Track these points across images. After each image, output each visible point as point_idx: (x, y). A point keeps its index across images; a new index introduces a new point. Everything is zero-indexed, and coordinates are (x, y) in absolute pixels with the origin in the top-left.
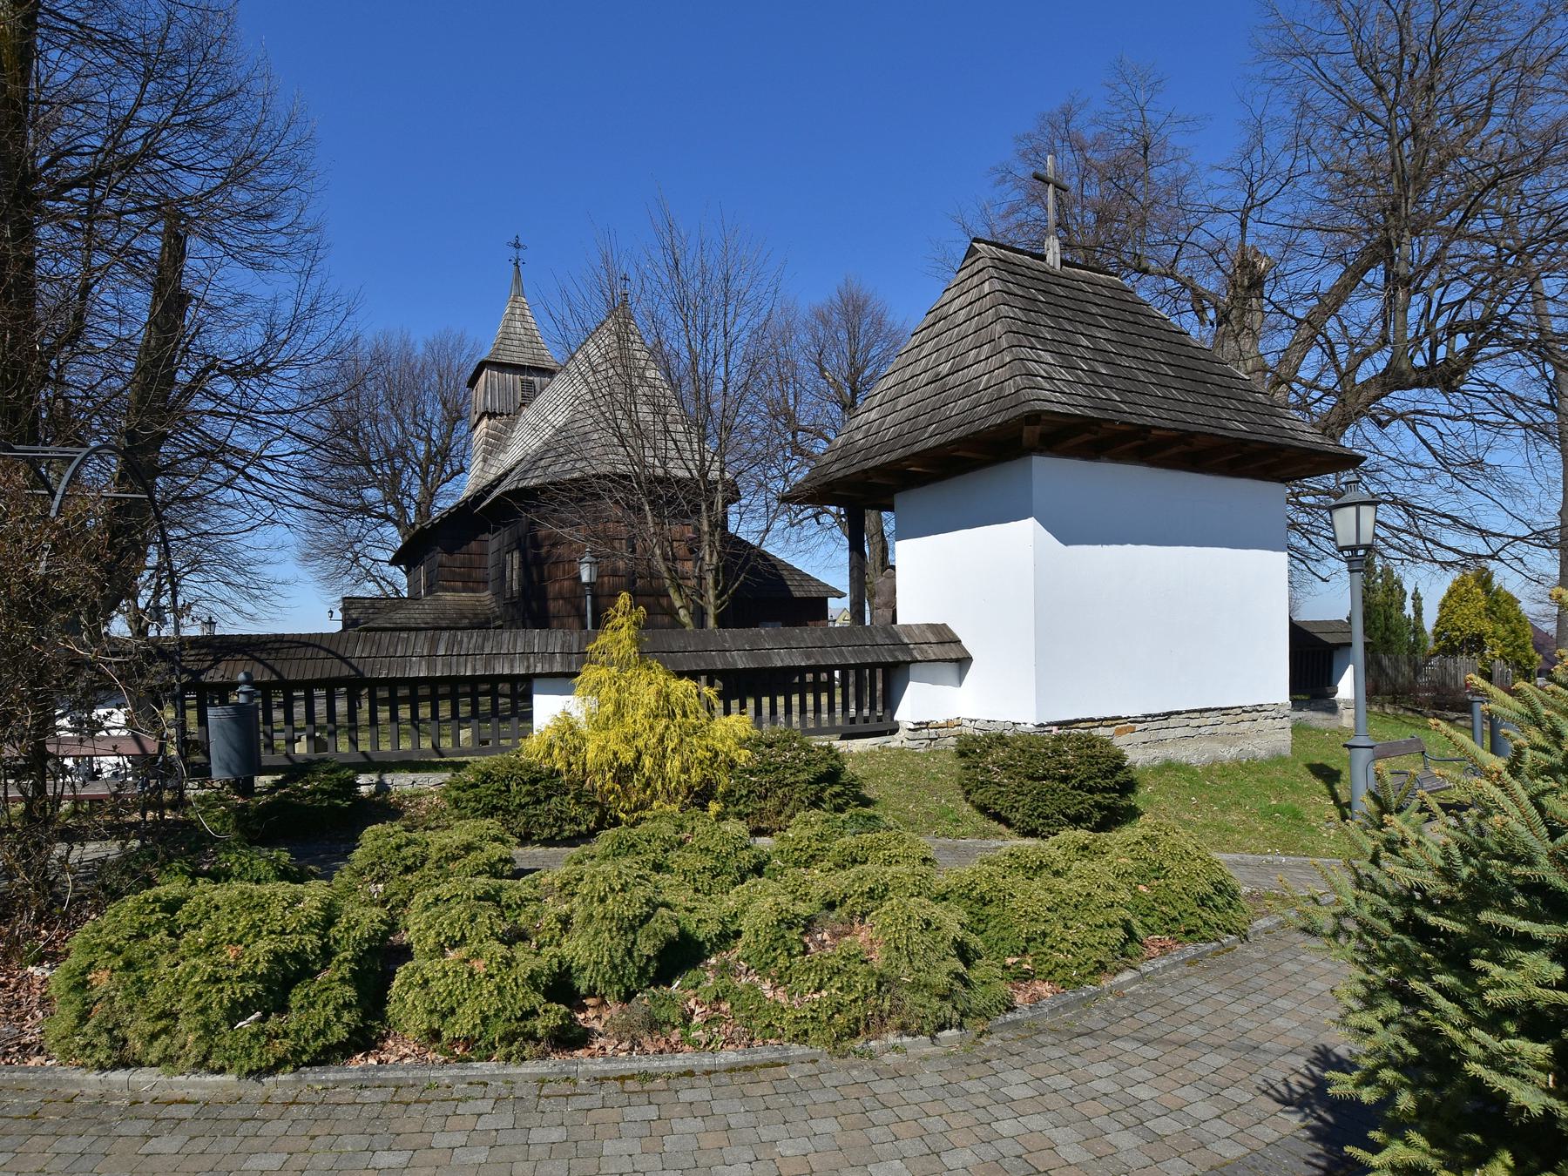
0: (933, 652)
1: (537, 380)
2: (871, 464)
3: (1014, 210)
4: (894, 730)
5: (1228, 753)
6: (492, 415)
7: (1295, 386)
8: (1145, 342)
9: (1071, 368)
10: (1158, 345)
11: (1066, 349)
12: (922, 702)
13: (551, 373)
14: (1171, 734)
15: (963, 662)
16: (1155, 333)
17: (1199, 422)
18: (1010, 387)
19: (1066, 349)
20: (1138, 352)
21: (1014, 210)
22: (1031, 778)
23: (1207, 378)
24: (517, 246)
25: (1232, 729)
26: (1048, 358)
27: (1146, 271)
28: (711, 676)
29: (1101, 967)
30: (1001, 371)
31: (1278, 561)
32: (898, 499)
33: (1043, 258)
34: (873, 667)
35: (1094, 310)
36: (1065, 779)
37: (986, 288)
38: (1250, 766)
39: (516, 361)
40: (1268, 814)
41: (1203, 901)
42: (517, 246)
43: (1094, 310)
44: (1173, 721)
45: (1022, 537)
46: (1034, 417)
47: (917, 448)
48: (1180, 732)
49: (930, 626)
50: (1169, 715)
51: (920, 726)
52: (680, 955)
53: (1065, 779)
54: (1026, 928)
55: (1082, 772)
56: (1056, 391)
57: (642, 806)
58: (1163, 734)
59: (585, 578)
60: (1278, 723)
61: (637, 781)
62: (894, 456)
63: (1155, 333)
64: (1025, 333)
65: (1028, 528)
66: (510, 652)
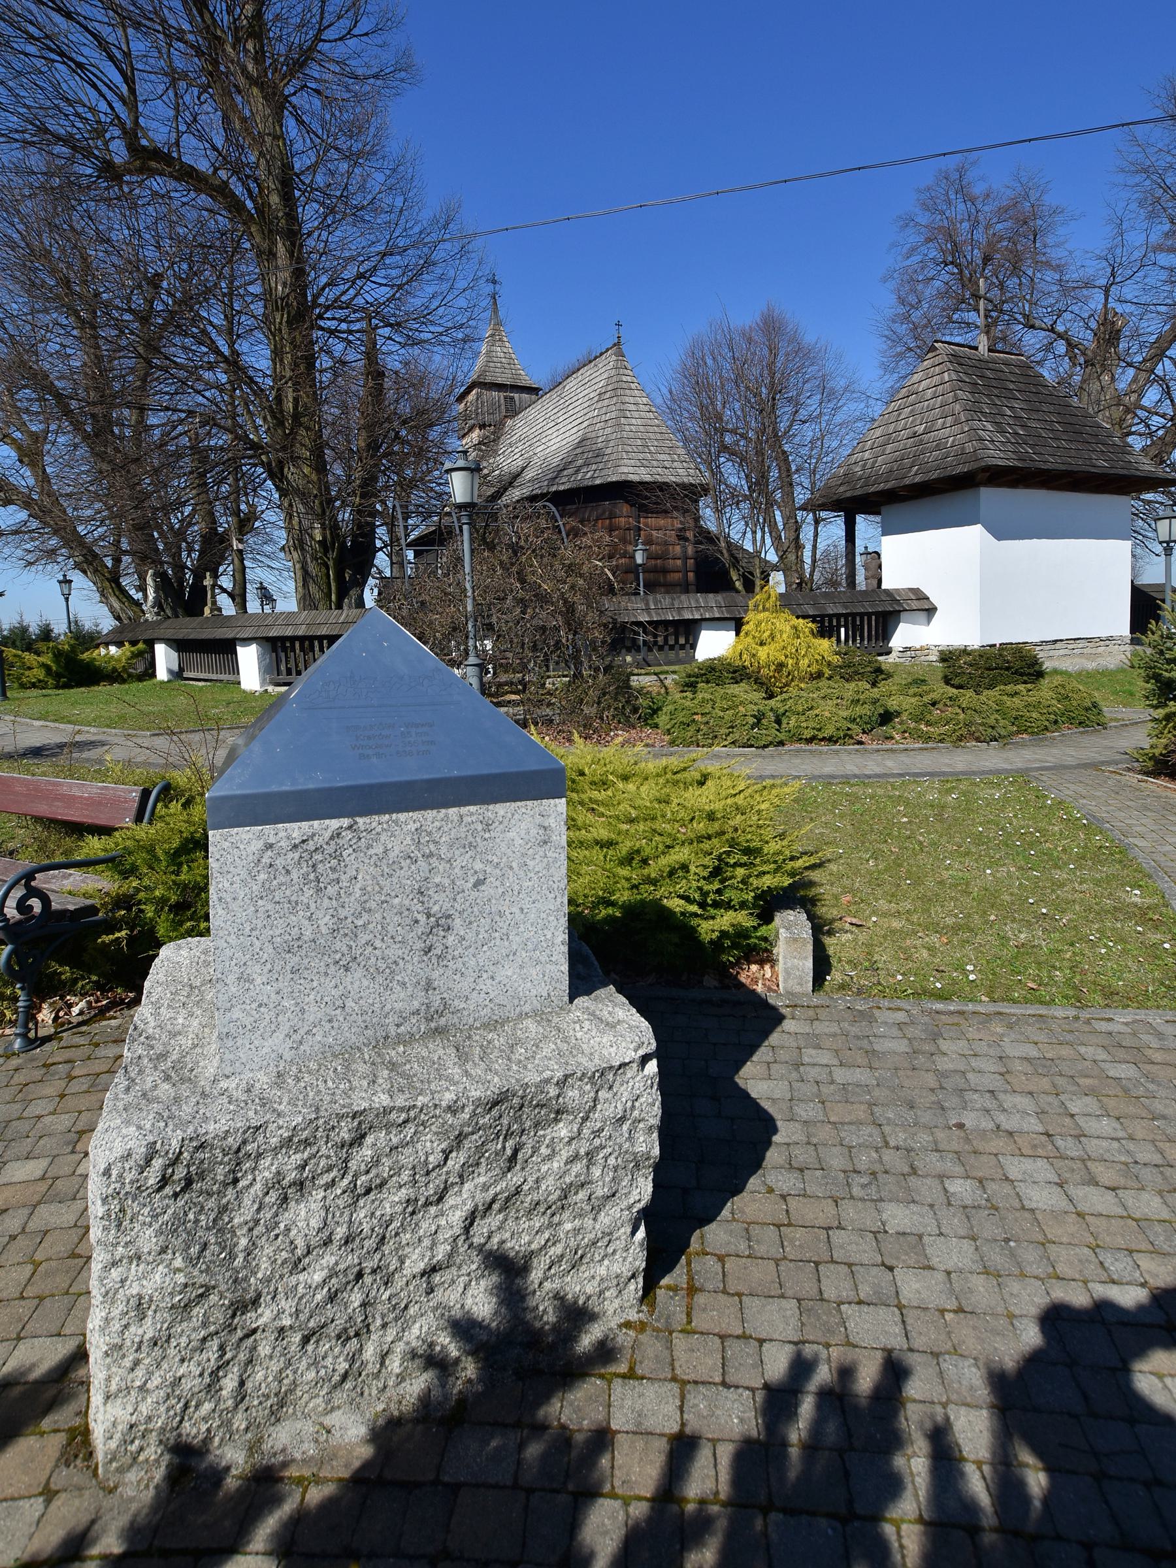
0: (915, 605)
1: (516, 396)
2: (872, 489)
3: (913, 250)
4: (889, 652)
5: (1091, 666)
6: (482, 426)
7: (1139, 412)
8: (1045, 407)
9: (1003, 432)
10: (1052, 408)
11: (999, 419)
12: (905, 636)
13: (533, 390)
14: (1057, 653)
15: (931, 611)
16: (1049, 399)
17: (1077, 463)
18: (969, 448)
19: (999, 419)
20: (1040, 416)
21: (913, 250)
22: (989, 669)
23: (1083, 430)
24: (494, 282)
25: (1094, 651)
26: (989, 426)
27: (1032, 327)
28: (814, 619)
29: (1046, 729)
30: (954, 433)
31: (1126, 546)
32: (884, 509)
33: (976, 348)
34: (862, 615)
35: (1012, 386)
36: (1007, 669)
37: (946, 376)
38: (1104, 673)
39: (500, 381)
40: (1116, 693)
41: (1087, 709)
42: (494, 282)
43: (1012, 386)
44: (1058, 645)
45: (974, 534)
46: (987, 469)
47: (907, 481)
48: (1062, 652)
49: (911, 590)
50: (1056, 641)
51: (907, 649)
52: (886, 718)
53: (1007, 669)
54: (1014, 713)
55: (1018, 664)
56: (998, 455)
57: (786, 685)
58: (1051, 653)
59: (639, 561)
60: (1122, 648)
61: (785, 672)
62: (889, 486)
63: (1049, 399)
64: (974, 410)
65: (978, 529)
66: (691, 606)
